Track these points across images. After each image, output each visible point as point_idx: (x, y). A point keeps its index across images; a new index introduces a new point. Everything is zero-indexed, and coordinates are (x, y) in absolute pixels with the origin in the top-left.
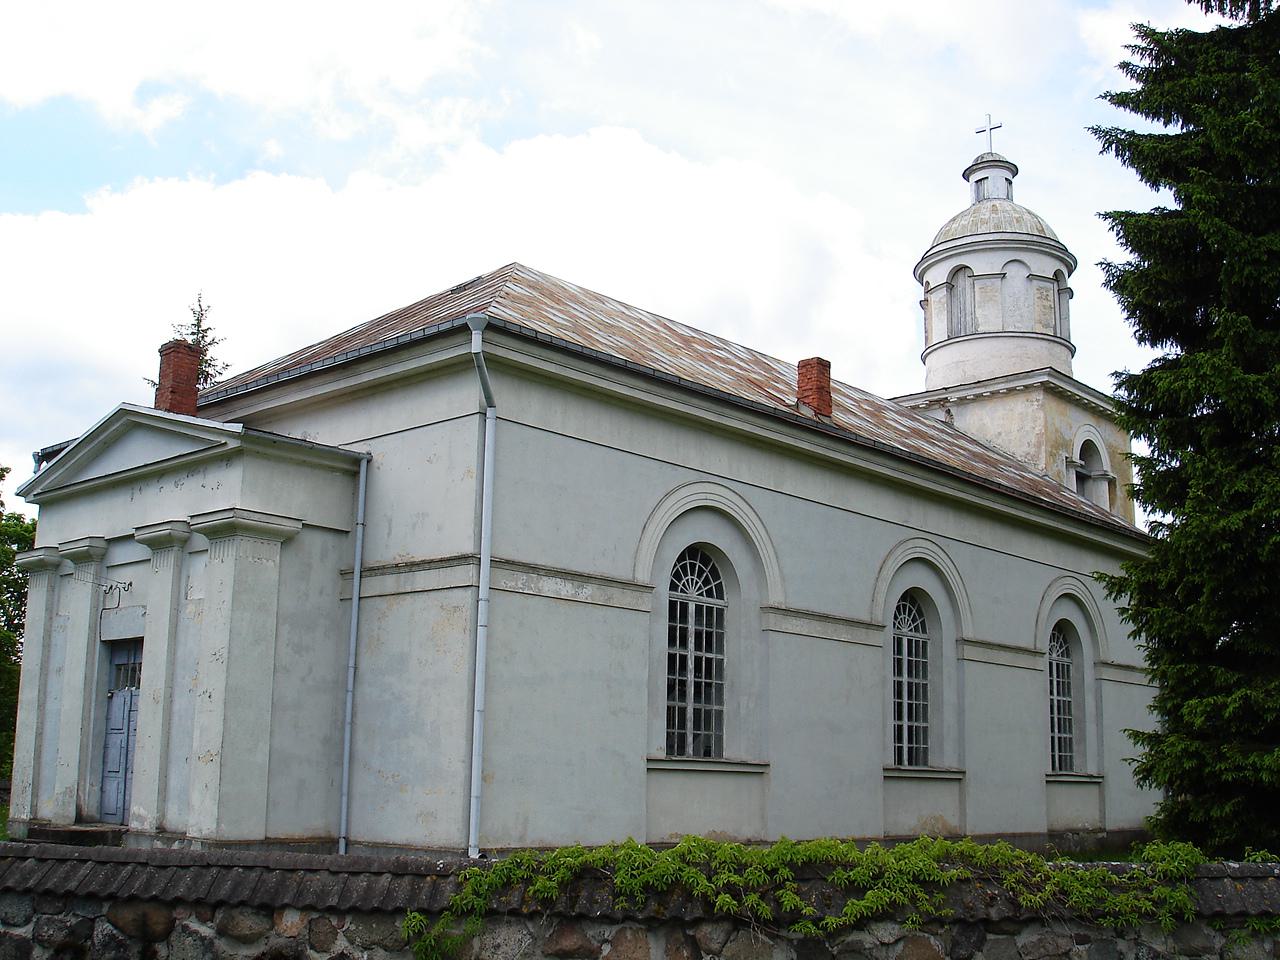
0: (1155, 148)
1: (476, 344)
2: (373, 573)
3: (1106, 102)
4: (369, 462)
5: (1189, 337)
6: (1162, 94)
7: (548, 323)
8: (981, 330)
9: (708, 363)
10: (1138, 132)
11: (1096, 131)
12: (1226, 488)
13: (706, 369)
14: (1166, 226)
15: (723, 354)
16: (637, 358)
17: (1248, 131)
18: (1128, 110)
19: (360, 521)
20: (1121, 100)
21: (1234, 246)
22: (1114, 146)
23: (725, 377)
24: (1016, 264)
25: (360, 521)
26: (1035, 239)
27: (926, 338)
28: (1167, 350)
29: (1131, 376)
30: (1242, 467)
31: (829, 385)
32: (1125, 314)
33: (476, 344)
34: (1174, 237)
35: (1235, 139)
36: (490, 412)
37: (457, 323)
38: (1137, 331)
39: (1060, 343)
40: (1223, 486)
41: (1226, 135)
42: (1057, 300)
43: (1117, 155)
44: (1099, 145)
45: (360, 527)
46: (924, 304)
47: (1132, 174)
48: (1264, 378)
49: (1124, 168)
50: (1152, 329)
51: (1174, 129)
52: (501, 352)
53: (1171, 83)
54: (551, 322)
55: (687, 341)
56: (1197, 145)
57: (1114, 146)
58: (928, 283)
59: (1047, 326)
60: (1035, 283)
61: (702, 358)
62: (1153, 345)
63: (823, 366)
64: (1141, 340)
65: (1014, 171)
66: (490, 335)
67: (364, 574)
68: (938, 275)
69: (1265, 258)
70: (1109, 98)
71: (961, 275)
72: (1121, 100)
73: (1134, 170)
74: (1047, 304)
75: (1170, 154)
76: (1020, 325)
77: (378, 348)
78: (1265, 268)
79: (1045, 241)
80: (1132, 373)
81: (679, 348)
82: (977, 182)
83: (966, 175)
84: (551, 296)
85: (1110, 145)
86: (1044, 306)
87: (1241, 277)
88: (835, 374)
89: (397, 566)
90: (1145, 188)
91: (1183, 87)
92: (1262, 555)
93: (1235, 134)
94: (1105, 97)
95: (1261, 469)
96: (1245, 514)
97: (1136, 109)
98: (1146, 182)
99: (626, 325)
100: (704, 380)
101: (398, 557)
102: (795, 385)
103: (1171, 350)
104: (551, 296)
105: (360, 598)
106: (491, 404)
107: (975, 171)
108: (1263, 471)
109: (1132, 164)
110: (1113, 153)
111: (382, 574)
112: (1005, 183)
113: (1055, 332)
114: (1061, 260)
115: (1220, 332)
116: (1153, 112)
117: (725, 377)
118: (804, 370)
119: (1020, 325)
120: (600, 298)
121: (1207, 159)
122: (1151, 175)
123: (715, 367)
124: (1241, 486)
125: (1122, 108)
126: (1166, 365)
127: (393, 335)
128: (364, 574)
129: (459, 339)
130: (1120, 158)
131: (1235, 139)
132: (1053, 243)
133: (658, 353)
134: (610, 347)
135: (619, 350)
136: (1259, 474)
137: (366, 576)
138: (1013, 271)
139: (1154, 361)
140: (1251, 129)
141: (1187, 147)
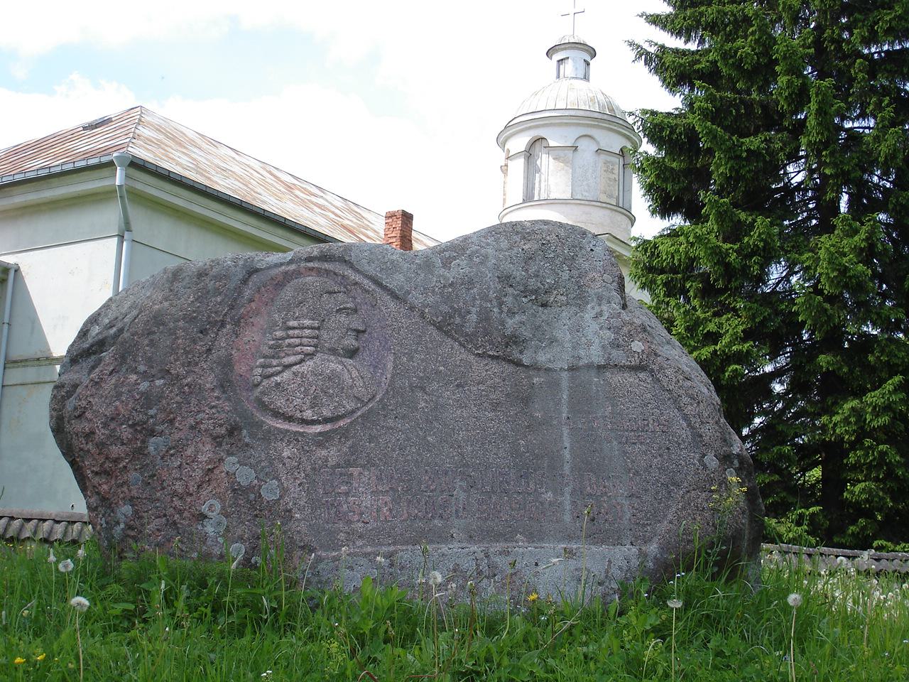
0: (674, 62)
1: (119, 178)
2: (16, 365)
3: (642, 20)
4: (16, 271)
5: (693, 213)
6: (684, 18)
7: (176, 163)
8: (552, 196)
9: (308, 208)
10: (667, 45)
11: (631, 44)
12: (701, 329)
13: (306, 213)
14: (676, 124)
15: (321, 201)
16: (249, 199)
17: (741, 55)
18: (658, 28)
19: (6, 320)
20: (655, 20)
21: (721, 144)
22: (643, 57)
23: (322, 221)
24: (588, 139)
25: (6, 320)
26: (605, 117)
27: (504, 200)
28: (672, 222)
29: (645, 241)
30: (716, 314)
31: (411, 235)
32: (642, 192)
33: (119, 178)
34: (681, 134)
35: (730, 61)
36: (127, 235)
37: (104, 159)
38: (650, 206)
39: (620, 212)
40: (700, 327)
41: (725, 56)
42: (621, 173)
43: (646, 64)
44: (632, 55)
45: (6, 326)
46: (504, 169)
47: (655, 80)
48: (736, 247)
49: (650, 75)
50: (664, 207)
51: (693, 46)
52: (139, 186)
53: (693, 10)
54: (178, 164)
55: (290, 188)
56: (708, 61)
57: (643, 57)
58: (509, 151)
59: (610, 196)
60: (603, 157)
61: (304, 203)
62: (663, 217)
63: (407, 218)
64: (653, 213)
65: (593, 54)
66: (133, 172)
67: (7, 366)
68: (519, 143)
69: (744, 155)
70: (645, 17)
71: (538, 144)
72: (655, 20)
73: (658, 78)
74: (613, 176)
75: (685, 67)
76: (587, 194)
77: (19, 177)
78: (744, 163)
79: (614, 120)
80: (646, 238)
81: (283, 193)
82: (559, 61)
83: (549, 53)
84: (173, 139)
85: (641, 56)
86: (610, 178)
87: (726, 169)
88: (416, 224)
89: (38, 359)
90: (663, 93)
91: (701, 14)
92: (723, 379)
93: (731, 57)
94: (642, 16)
95: (729, 316)
96: (712, 348)
97: (664, 27)
98: (666, 88)
99: (236, 169)
100: (303, 222)
101: (39, 353)
102: (382, 233)
103: (677, 221)
104: (173, 139)
105: (3, 386)
106: (129, 230)
107: (557, 51)
108: (732, 317)
109: (656, 72)
110: (642, 62)
111: (24, 366)
112: (583, 64)
113: (618, 202)
114: (628, 138)
115: (706, 210)
116: (678, 33)
117: (322, 221)
118: (390, 220)
119: (587, 194)
120: (466, 239)
121: (711, 77)
122: (669, 83)
123: (313, 212)
124: (711, 327)
125: (653, 26)
126: (674, 234)
127: (36, 165)
128: (7, 366)
129: (105, 172)
130: (647, 67)
131: (730, 61)
132: (621, 122)
133: (272, 200)
134: (228, 188)
135: (234, 191)
136: (728, 319)
137: (9, 368)
138: (583, 144)
139: (663, 230)
140: (744, 55)
141: (698, 62)
